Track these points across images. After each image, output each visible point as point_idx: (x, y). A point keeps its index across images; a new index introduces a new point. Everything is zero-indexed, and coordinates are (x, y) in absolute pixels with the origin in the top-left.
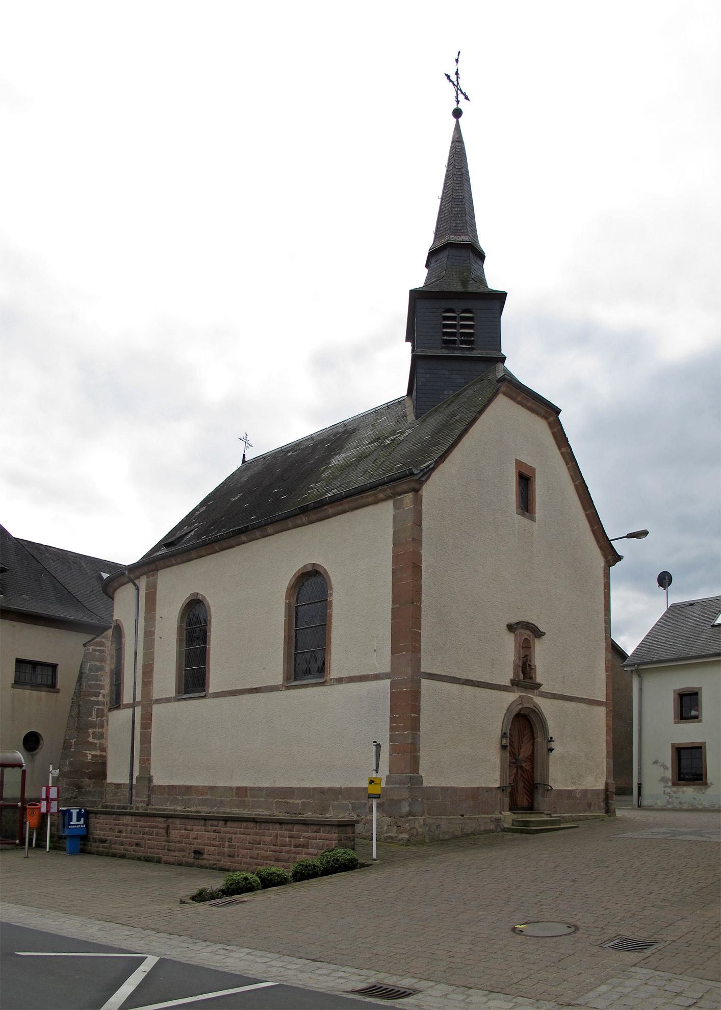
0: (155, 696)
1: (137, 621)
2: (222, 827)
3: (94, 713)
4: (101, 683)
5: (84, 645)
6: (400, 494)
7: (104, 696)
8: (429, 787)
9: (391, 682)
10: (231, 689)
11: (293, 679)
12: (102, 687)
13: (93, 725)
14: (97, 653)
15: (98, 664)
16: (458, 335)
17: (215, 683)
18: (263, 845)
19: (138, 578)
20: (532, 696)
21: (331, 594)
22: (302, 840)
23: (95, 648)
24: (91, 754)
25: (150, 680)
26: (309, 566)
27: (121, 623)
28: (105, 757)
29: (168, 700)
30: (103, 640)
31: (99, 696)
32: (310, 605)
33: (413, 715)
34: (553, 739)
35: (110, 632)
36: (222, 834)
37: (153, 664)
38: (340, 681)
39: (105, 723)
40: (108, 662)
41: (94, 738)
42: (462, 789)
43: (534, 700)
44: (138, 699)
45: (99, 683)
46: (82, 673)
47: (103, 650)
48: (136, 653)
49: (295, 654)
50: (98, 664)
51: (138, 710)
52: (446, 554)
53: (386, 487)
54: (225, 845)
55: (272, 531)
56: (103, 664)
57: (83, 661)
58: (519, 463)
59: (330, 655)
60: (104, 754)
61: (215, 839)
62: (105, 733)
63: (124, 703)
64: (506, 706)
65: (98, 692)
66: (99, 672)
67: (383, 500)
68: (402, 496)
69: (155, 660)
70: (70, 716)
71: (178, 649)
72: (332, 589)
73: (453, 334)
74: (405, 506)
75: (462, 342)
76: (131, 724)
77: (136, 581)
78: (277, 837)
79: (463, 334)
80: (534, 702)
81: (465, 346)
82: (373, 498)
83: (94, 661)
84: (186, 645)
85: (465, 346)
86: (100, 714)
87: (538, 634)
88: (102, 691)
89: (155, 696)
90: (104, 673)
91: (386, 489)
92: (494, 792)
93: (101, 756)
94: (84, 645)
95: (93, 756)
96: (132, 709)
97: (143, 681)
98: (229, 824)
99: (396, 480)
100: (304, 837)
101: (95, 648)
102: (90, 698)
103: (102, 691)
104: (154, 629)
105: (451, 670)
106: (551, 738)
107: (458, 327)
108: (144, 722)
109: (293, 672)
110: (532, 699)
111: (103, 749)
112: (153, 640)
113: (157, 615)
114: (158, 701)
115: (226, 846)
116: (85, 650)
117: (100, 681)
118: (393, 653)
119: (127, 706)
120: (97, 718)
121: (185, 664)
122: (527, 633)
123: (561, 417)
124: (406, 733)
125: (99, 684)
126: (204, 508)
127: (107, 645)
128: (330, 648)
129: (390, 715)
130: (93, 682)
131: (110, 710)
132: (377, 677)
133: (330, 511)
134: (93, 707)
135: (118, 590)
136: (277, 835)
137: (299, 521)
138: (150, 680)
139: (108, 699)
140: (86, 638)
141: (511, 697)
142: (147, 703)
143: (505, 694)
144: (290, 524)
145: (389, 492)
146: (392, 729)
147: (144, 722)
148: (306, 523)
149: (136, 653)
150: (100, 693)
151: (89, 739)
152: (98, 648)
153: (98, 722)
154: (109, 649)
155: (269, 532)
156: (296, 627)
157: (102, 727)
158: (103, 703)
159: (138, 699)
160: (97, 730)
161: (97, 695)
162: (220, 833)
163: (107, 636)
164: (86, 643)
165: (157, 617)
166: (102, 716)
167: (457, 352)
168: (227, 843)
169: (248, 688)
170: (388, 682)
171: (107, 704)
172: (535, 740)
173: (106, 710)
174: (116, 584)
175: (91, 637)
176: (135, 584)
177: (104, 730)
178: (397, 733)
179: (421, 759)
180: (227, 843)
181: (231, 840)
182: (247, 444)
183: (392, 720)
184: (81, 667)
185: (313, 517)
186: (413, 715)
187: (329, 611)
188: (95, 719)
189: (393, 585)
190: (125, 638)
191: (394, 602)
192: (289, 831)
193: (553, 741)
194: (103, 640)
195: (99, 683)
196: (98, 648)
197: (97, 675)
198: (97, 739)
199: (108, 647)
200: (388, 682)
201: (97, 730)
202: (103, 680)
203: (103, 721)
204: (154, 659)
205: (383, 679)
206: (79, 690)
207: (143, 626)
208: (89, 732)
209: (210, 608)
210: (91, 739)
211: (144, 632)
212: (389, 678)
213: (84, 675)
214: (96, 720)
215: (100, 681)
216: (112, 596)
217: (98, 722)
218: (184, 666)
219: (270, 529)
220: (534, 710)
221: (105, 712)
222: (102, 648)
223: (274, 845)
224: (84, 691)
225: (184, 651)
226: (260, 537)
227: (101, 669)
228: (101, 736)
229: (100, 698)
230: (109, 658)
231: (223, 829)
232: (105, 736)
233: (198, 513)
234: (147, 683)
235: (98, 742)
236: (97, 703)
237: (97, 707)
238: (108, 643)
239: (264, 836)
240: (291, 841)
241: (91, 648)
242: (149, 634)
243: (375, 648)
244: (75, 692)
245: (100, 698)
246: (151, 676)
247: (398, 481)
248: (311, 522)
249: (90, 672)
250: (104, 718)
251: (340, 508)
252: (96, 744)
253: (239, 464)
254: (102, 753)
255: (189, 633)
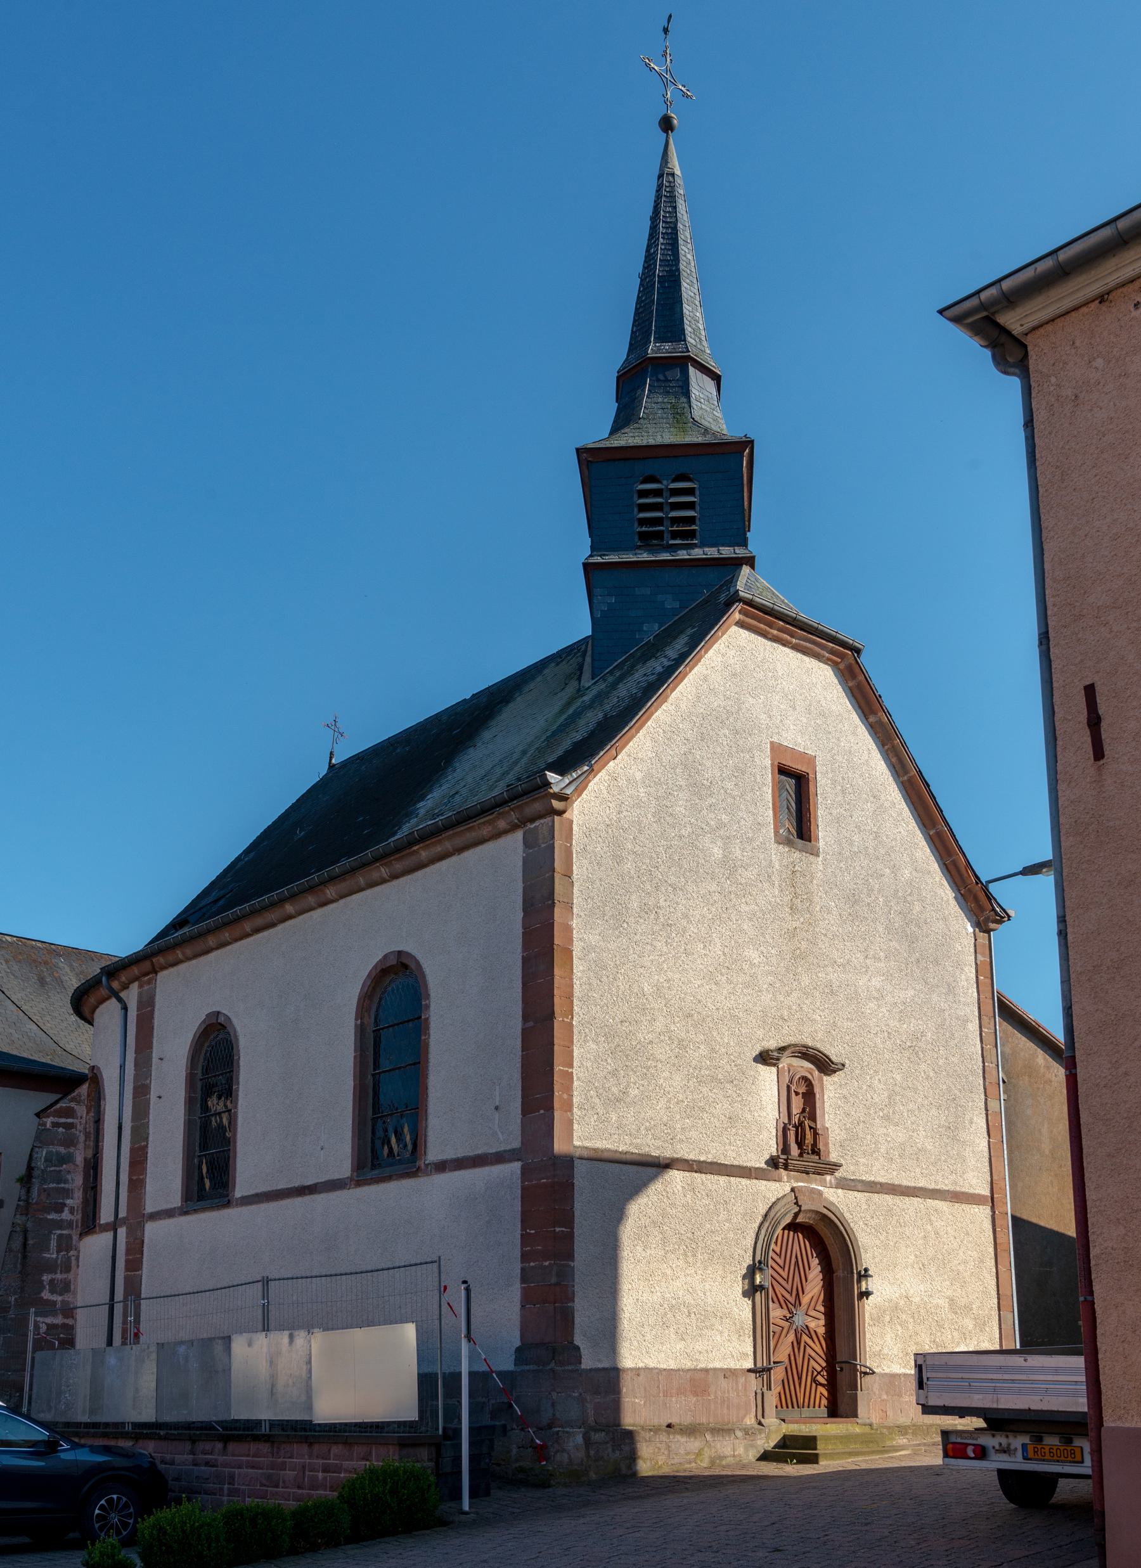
0: (150, 1208)
1: (122, 1067)
2: (218, 1455)
3: (53, 1244)
4: (66, 1186)
5: (38, 1115)
6: (532, 820)
7: (72, 1212)
8: (598, 1370)
9: (523, 1169)
10: (269, 1189)
11: (370, 1166)
12: (67, 1193)
13: (51, 1267)
14: (61, 1130)
15: (62, 1150)
16: (667, 523)
17: (244, 1181)
18: (282, 1487)
19: (125, 987)
20: (820, 1188)
21: (428, 1007)
22: (342, 1475)
23: (56, 1120)
24: (46, 1324)
25: (141, 1177)
26: (392, 957)
27: (101, 1072)
28: (72, 1328)
29: (169, 1213)
30: (73, 1104)
31: (62, 1211)
32: (401, 1025)
33: (558, 1229)
34: (870, 1272)
35: (84, 1089)
36: (219, 1469)
37: (147, 1146)
38: (442, 1167)
39: (74, 1262)
40: (81, 1146)
41: (52, 1292)
42: (670, 1372)
43: (826, 1195)
44: (122, 1214)
45: (62, 1185)
46: (32, 1169)
47: (73, 1123)
48: (120, 1128)
49: (373, 1119)
50: (62, 1150)
51: (122, 1232)
52: (625, 925)
53: (507, 808)
54: (222, 1489)
55: (333, 894)
56: (72, 1151)
57: (33, 1146)
58: (776, 748)
59: (426, 1119)
60: (70, 1322)
61: (207, 1479)
62: (72, 1282)
63: (101, 1222)
64: (762, 1209)
65: (61, 1203)
66: (64, 1166)
67: (506, 832)
68: (537, 823)
69: (151, 1139)
70: (9, 1250)
71: (187, 1117)
72: (428, 997)
73: (658, 521)
74: (541, 841)
75: (675, 535)
76: (110, 1263)
77: (123, 995)
78: (304, 1473)
79: (675, 521)
80: (826, 1199)
81: (680, 542)
82: (490, 828)
83: (53, 1144)
84: (201, 1108)
85: (680, 542)
86: (66, 1245)
87: (825, 1065)
88: (68, 1202)
89: (150, 1208)
90: (73, 1166)
91: (508, 812)
92: (742, 1380)
93: (65, 1326)
94: (38, 1115)
95: (50, 1327)
96: (112, 1233)
97: (130, 1180)
98: (231, 1446)
99: (522, 796)
100: (346, 1471)
101: (56, 1120)
102: (45, 1215)
103: (68, 1202)
104: (148, 1082)
105: (639, 1141)
106: (866, 1270)
107: (666, 508)
108: (131, 1257)
109: (370, 1154)
110: (820, 1193)
111: (69, 1311)
112: (147, 1103)
113: (154, 1055)
114: (155, 1216)
115: (226, 1491)
116: (39, 1124)
117: (66, 1181)
118: (524, 1113)
119: (106, 1228)
120: (58, 1252)
121: (200, 1144)
122: (805, 1067)
123: (864, 659)
124: (547, 1263)
125: (63, 1188)
126: (251, 855)
127: (79, 1115)
128: (426, 1106)
129: (521, 1231)
130: (51, 1185)
131: (82, 1235)
132: (499, 1158)
133: (424, 855)
134: (50, 1232)
135: (98, 1011)
136: (304, 1467)
137: (375, 875)
138: (141, 1177)
139: (79, 1217)
140: (44, 1099)
141: (777, 1189)
142: (137, 1219)
143: (762, 1185)
144: (362, 881)
145: (514, 817)
146: (525, 1257)
147: (131, 1257)
148: (388, 878)
149: (120, 1128)
150: (65, 1205)
151: (43, 1294)
152: (63, 1120)
153: (59, 1262)
154: (83, 1121)
155: (329, 896)
156: (374, 1070)
157: (67, 1268)
158: (70, 1224)
159: (122, 1214)
160: (59, 1276)
161: (59, 1208)
162: (217, 1466)
163: (80, 1096)
164: (42, 1111)
165: (155, 1060)
166: (69, 1248)
167: (665, 554)
168: (226, 1486)
169: (296, 1185)
170: (517, 1166)
171: (77, 1226)
172: (835, 1275)
173: (75, 1238)
174: (92, 1000)
175: (52, 1097)
176: (120, 1000)
177: (71, 1276)
178: (532, 1264)
179: (576, 1314)
180: (226, 1486)
181: (234, 1480)
182: (336, 734)
183: (524, 1238)
184: (31, 1156)
185: (398, 866)
186: (558, 1229)
187: (423, 1038)
188: (54, 1256)
189: (524, 984)
190: (105, 1099)
191: (525, 1018)
192: (323, 1458)
193: (871, 1276)
194: (73, 1104)
195: (62, 1185)
196: (63, 1120)
197: (60, 1171)
198: (57, 1293)
199: (81, 1118)
200: (517, 1166)
201: (59, 1276)
202: (70, 1179)
203: (69, 1258)
204: (148, 1138)
205: (510, 1161)
206: (27, 1201)
207: (132, 1077)
208: (43, 1281)
209: (237, 1040)
210: (46, 1295)
211: (134, 1087)
212: (518, 1160)
213: (36, 1173)
214: (57, 1258)
215: (66, 1181)
216: (90, 1019)
217: (59, 1262)
218: (197, 1148)
219: (330, 892)
220: (825, 1216)
221: (74, 1243)
222: (70, 1120)
223: (299, 1487)
224: (35, 1204)
225: (198, 1121)
226: (316, 906)
227: (68, 1159)
228: (66, 1287)
229: (66, 1215)
230: (82, 1138)
231: (221, 1459)
232: (72, 1287)
233: (240, 864)
234: (137, 1185)
235: (60, 1298)
236: (59, 1224)
237: (59, 1232)
238: (81, 1110)
239: (285, 1470)
240: (325, 1479)
241: (49, 1121)
242: (142, 1091)
243: (497, 1104)
244: (18, 1205)
245: (66, 1215)
246: (143, 1171)
247: (534, 793)
248: (395, 876)
249: (47, 1167)
250: (71, 1253)
251: (439, 849)
252: (55, 1303)
253: (324, 771)
254: (66, 1321)
255: (206, 1086)
